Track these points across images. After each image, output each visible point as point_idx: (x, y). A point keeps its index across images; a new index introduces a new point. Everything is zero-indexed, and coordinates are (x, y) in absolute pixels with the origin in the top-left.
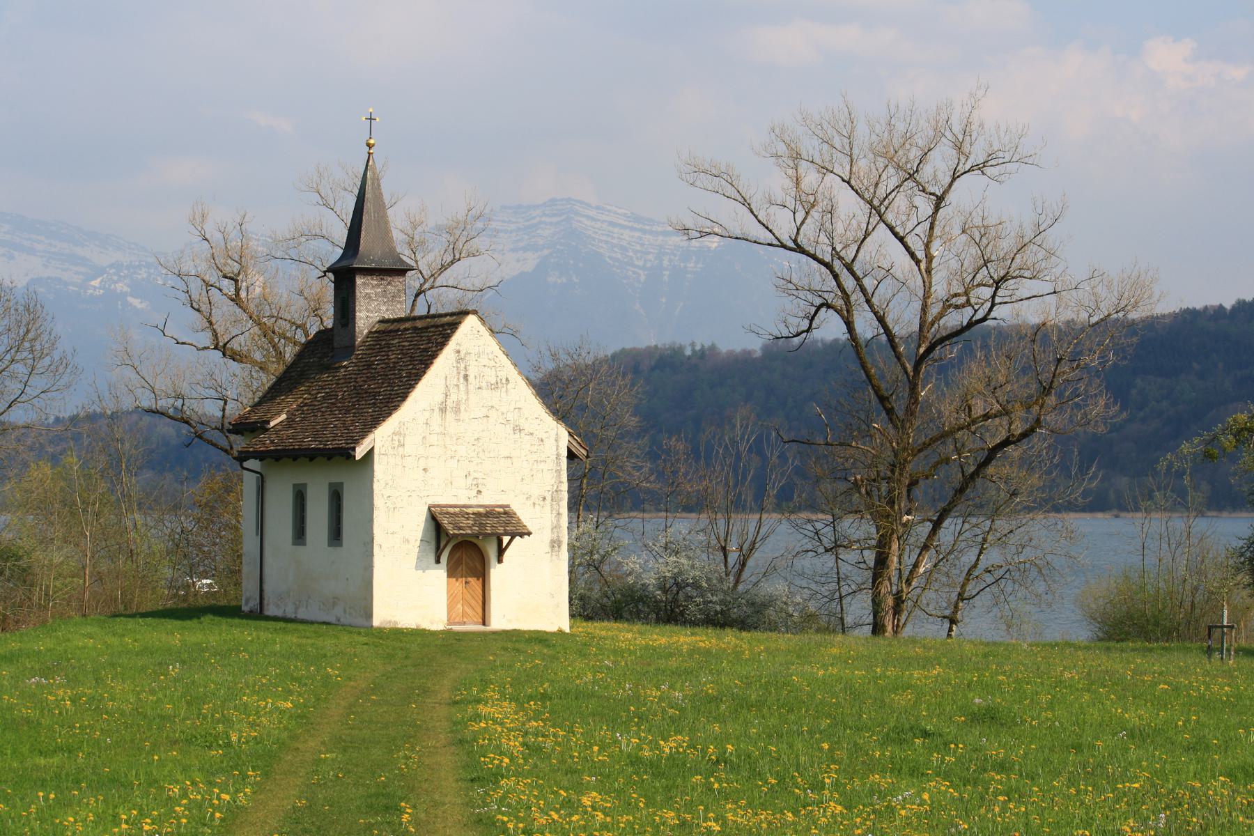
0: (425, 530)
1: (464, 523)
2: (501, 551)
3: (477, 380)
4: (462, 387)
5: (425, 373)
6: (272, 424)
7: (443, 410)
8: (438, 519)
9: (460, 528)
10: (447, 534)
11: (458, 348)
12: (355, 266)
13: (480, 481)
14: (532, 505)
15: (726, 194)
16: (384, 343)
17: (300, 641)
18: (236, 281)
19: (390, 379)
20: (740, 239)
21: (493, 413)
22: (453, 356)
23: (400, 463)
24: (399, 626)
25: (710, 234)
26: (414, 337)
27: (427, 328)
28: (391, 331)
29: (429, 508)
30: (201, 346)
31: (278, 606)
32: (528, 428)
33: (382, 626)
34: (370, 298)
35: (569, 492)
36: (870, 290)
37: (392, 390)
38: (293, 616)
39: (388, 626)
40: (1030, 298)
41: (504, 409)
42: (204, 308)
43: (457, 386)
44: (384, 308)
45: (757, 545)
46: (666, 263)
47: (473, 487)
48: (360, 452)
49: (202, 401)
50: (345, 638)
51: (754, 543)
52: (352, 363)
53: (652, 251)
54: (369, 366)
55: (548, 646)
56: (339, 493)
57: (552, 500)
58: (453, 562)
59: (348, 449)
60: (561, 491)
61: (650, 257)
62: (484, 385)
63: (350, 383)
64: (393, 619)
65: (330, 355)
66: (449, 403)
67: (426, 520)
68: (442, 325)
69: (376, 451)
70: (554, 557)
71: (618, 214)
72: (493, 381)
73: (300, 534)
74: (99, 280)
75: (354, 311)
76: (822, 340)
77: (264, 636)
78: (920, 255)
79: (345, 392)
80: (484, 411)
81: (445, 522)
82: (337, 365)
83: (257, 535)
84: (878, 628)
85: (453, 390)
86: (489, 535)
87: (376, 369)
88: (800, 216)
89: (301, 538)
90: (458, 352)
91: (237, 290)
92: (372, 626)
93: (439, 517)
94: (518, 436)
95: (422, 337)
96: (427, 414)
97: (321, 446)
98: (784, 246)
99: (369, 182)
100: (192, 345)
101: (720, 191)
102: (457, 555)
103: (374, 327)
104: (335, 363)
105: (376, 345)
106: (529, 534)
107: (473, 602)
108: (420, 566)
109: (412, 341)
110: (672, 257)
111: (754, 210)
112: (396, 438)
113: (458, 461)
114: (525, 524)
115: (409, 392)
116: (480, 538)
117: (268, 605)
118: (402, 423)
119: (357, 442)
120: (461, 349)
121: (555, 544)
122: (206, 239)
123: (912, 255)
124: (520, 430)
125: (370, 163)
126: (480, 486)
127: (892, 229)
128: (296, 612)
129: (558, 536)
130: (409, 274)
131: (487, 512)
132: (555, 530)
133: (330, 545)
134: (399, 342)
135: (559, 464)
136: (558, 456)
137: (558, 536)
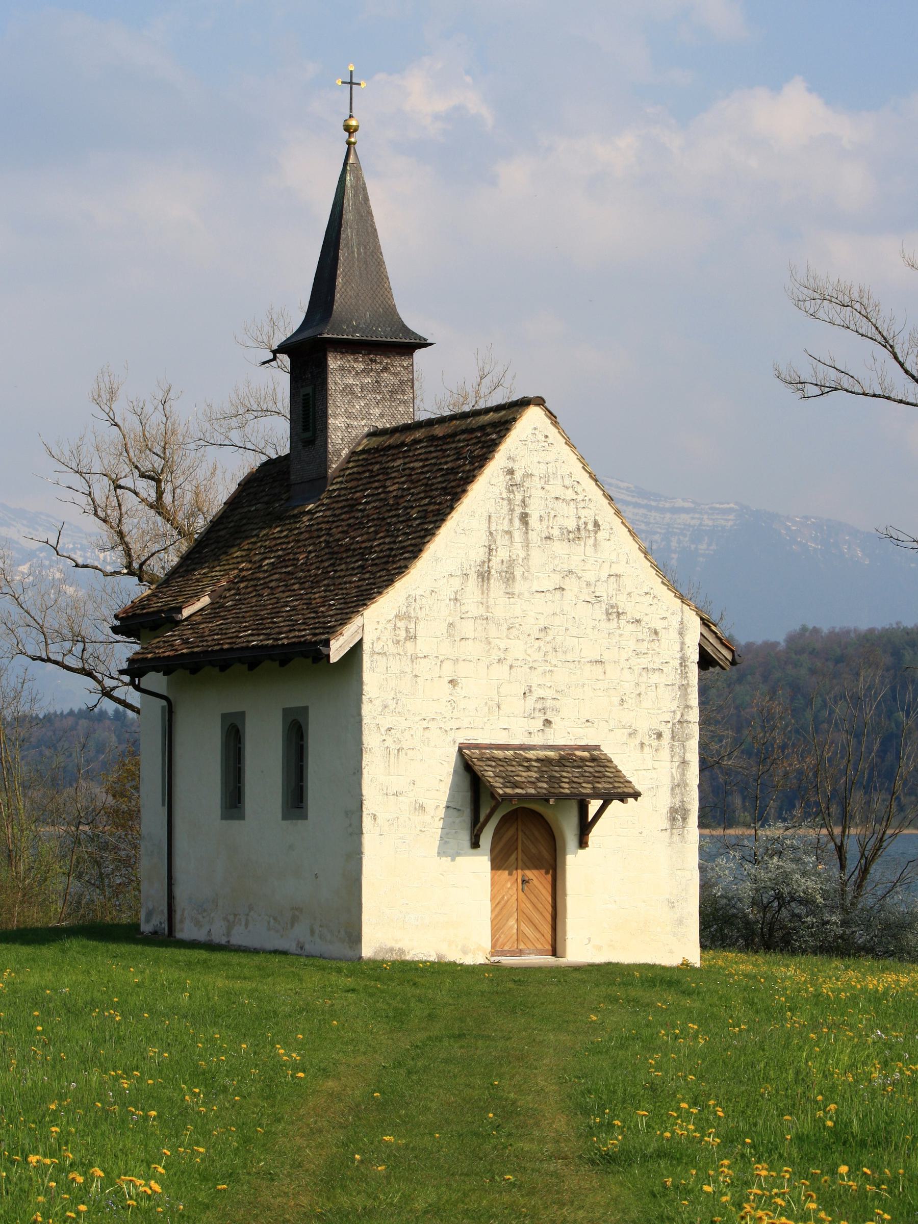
0: (454, 788)
1: (523, 775)
2: (585, 828)
3: (545, 523)
4: (518, 536)
5: (452, 508)
6: (186, 613)
7: (484, 576)
8: (476, 768)
9: (516, 785)
10: (493, 795)
11: (510, 465)
12: (326, 336)
13: (549, 703)
14: (639, 747)
15: (860, 331)
16: (377, 467)
17: (230, 984)
18: (158, 481)
19: (389, 524)
20: (879, 396)
21: (571, 584)
22: (502, 480)
23: (409, 670)
24: (408, 958)
25: (836, 389)
26: (430, 452)
27: (454, 435)
28: (390, 447)
29: (460, 750)
30: (109, 569)
31: (198, 924)
32: (631, 609)
33: (379, 958)
34: (352, 393)
37: (394, 542)
38: (223, 941)
39: (388, 957)
40: (276, 952)
41: (590, 576)
42: (114, 515)
43: (509, 533)
44: (377, 411)
45: (885, 844)
46: (674, 544)
47: (537, 714)
48: (337, 649)
49: (111, 646)
50: (313, 979)
51: (881, 840)
52: (323, 505)
53: (659, 530)
54: (352, 506)
55: (688, 993)
56: (300, 727)
57: (673, 738)
58: (501, 844)
59: (316, 643)
60: (688, 722)
61: (657, 537)
62: (556, 532)
63: (319, 537)
64: (397, 946)
65: (284, 496)
66: (495, 563)
67: (455, 771)
68: (482, 428)
69: (366, 647)
70: (676, 838)
71: (620, 488)
74: (27, 565)
75: (325, 416)
76: (855, 630)
77: (165, 974)
79: (310, 552)
80: (556, 580)
81: (489, 774)
82: (296, 512)
83: (163, 805)
85: (501, 540)
86: (567, 797)
87: (365, 510)
89: (236, 807)
90: (511, 472)
91: (160, 494)
92: (361, 957)
93: (478, 766)
94: (614, 624)
95: (446, 450)
96: (456, 583)
97: (270, 642)
99: (349, 193)
100: (96, 568)
101: (852, 327)
103: (359, 444)
104: (294, 509)
105: (364, 472)
106: (636, 795)
107: (536, 917)
108: (446, 849)
109: (427, 459)
110: (681, 538)
111: (899, 355)
112: (401, 624)
113: (511, 667)
114: (630, 779)
115: (424, 544)
116: (552, 801)
117: (182, 922)
118: (411, 600)
119: (333, 631)
120: (516, 467)
121: (677, 814)
122: (116, 425)
124: (619, 614)
125: (351, 161)
126: (549, 712)
128: (228, 934)
129: (683, 802)
130: (419, 354)
131: (562, 758)
132: (677, 790)
133: (285, 817)
134: (405, 464)
135: (684, 675)
137: (683, 802)
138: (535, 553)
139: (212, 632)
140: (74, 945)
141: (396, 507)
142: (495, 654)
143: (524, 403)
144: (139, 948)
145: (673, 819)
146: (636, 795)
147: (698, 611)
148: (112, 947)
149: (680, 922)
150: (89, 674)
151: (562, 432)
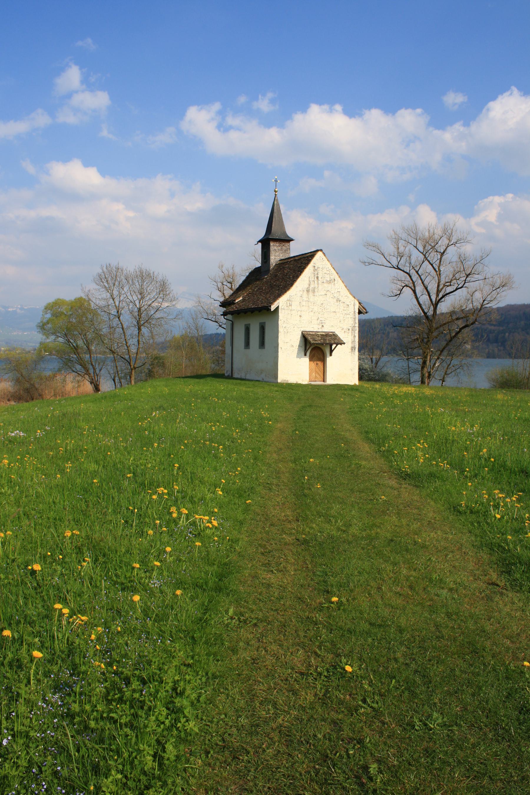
1: (317, 338)
2: (331, 351)
4: (316, 282)
5: (300, 275)
6: (237, 301)
7: (308, 291)
9: (316, 341)
10: (310, 343)
17: (246, 389)
18: (231, 283)
21: (328, 293)
22: (312, 269)
35: (359, 327)
36: (423, 280)
40: (257, 381)
41: (333, 292)
48: (273, 308)
54: (276, 276)
62: (325, 281)
66: (310, 288)
68: (307, 257)
69: (280, 307)
72: (329, 280)
73: (247, 344)
75: (269, 256)
77: (230, 387)
78: (437, 270)
80: (325, 292)
84: (423, 382)
88: (399, 259)
90: (314, 267)
91: (232, 286)
93: (307, 336)
96: (301, 293)
98: (394, 268)
99: (275, 206)
102: (313, 352)
106: (344, 343)
107: (319, 372)
108: (298, 356)
119: (272, 303)
121: (353, 348)
123: (435, 269)
127: (429, 261)
128: (245, 376)
130: (291, 242)
135: (355, 315)
136: (354, 312)
138: (320, 286)
139: (243, 305)
140: (209, 379)
141: (286, 275)
142: (310, 310)
143: (317, 251)
144: (224, 380)
145: (352, 350)
146: (344, 343)
147: (358, 301)
148: (217, 379)
149: (354, 374)
150: (217, 322)
151: (326, 258)
